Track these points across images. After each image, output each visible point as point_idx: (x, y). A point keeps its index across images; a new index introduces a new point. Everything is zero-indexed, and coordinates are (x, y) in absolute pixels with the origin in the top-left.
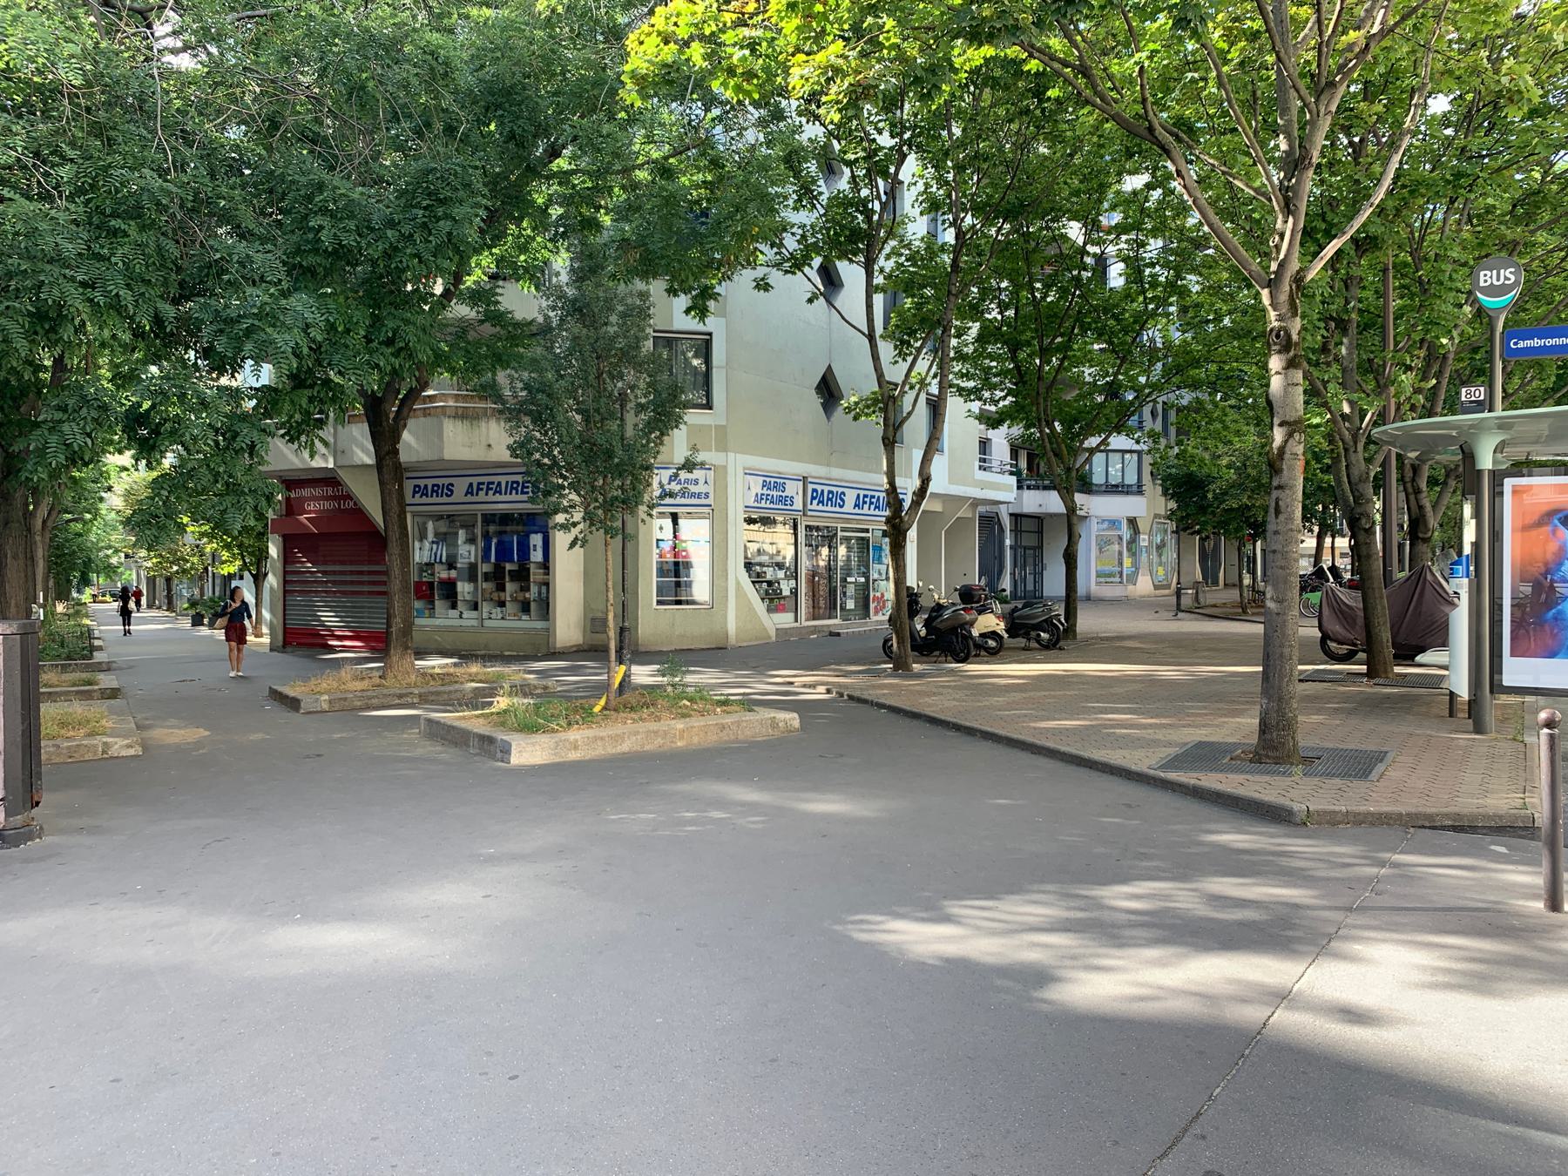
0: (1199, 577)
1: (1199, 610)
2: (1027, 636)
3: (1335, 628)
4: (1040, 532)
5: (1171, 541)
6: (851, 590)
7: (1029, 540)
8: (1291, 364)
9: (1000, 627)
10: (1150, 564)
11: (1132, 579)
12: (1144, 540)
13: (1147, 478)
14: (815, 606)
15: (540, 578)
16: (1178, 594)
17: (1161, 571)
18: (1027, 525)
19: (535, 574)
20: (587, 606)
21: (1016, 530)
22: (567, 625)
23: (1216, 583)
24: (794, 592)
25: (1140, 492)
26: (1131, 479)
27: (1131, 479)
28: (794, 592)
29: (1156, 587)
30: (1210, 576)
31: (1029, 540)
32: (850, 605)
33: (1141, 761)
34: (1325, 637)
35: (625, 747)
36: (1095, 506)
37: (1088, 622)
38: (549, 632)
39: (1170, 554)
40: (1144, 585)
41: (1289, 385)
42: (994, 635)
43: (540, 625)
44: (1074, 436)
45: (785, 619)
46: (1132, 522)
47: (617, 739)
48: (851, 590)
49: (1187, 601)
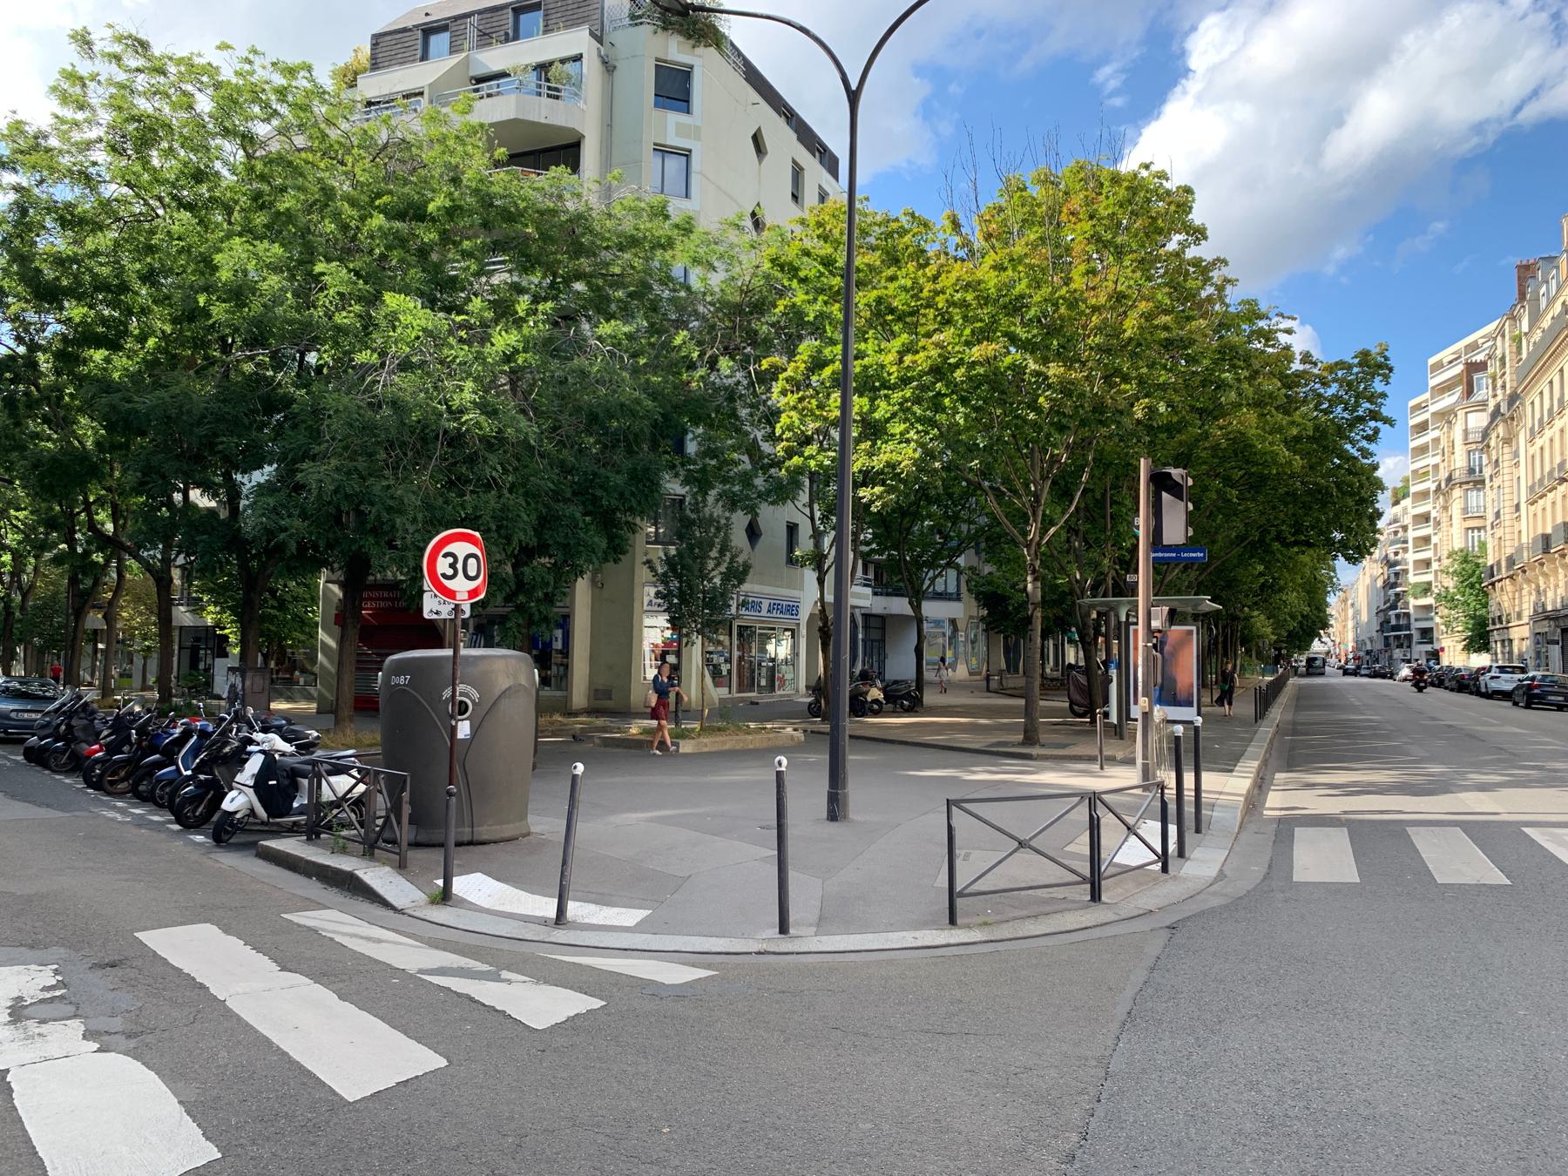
0: (1003, 665)
1: (1002, 691)
2: (895, 703)
3: (1077, 697)
4: (883, 629)
5: (982, 638)
6: (764, 671)
7: (875, 635)
8: (1035, 579)
9: (881, 696)
10: (966, 653)
11: (953, 666)
12: (961, 637)
13: (964, 588)
14: (740, 684)
15: (559, 660)
16: (988, 679)
17: (974, 661)
18: (873, 623)
19: (556, 658)
20: (591, 682)
21: (866, 627)
22: (579, 694)
23: (1017, 671)
24: (729, 672)
25: (958, 599)
26: (952, 589)
27: (952, 589)
28: (729, 672)
29: (971, 674)
30: (1012, 666)
31: (875, 635)
32: (763, 683)
33: (976, 746)
34: (1072, 703)
35: (727, 747)
36: (930, 609)
37: (929, 698)
38: (567, 699)
39: (982, 647)
40: (962, 672)
41: (1035, 588)
42: (876, 701)
43: (558, 693)
44: (918, 564)
45: (723, 692)
46: (953, 622)
47: (724, 743)
48: (764, 671)
49: (993, 685)
